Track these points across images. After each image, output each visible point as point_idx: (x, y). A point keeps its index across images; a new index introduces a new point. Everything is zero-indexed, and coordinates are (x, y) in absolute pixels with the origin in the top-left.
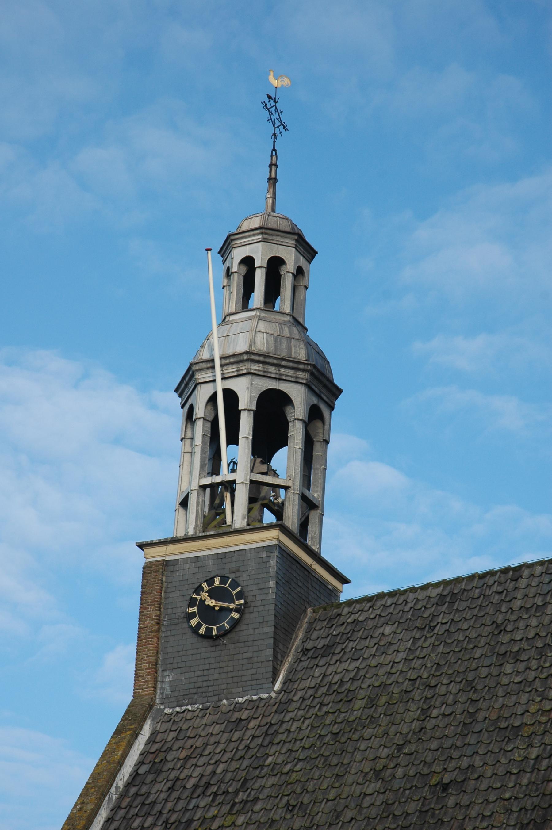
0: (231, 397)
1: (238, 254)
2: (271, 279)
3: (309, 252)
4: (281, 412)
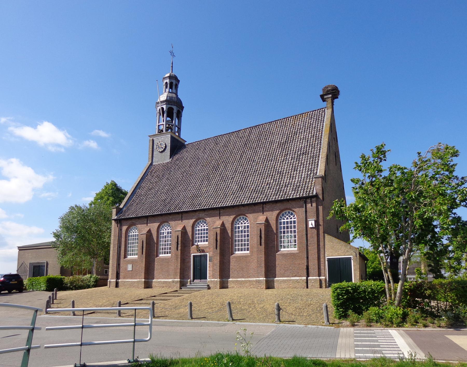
0: (163, 108)
1: (165, 81)
2: (174, 83)
3: (179, 81)
4: (174, 109)
